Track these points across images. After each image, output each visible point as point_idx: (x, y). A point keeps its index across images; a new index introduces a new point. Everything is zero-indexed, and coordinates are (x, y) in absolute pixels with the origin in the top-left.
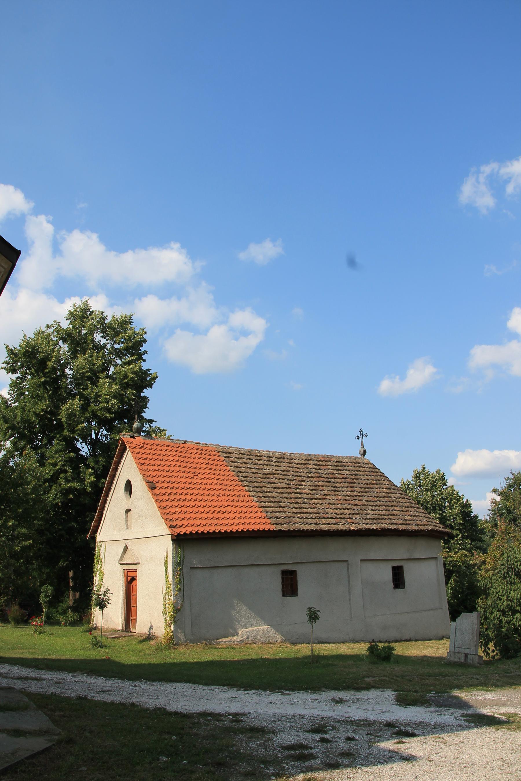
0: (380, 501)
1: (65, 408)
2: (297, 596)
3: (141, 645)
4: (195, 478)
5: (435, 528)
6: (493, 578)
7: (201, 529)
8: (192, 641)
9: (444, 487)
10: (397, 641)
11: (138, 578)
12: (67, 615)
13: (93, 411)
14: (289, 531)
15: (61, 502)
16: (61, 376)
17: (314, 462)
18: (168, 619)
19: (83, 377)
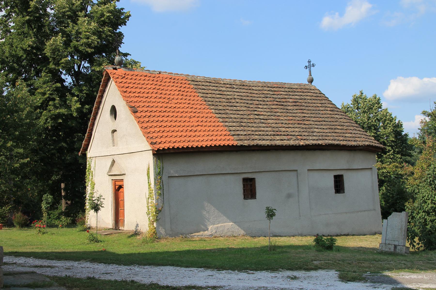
0: (324, 121)
1: (49, 44)
2: (256, 199)
3: (129, 240)
4: (170, 103)
5: (371, 144)
6: (420, 185)
7: (176, 145)
8: (171, 236)
9: (380, 110)
10: (337, 236)
11: (124, 187)
12: (61, 219)
14: (249, 146)
15: (51, 126)
16: (43, 15)
17: (269, 89)
18: (151, 218)
19: (64, 16)
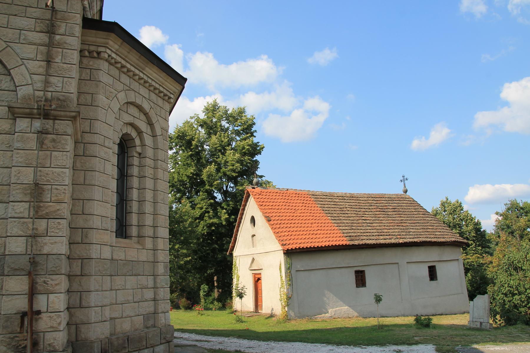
3: (267, 321)
7: (302, 246)
8: (299, 317)
10: (433, 315)
11: (262, 279)
13: (224, 172)
14: (359, 245)
17: (373, 199)
18: (283, 304)
